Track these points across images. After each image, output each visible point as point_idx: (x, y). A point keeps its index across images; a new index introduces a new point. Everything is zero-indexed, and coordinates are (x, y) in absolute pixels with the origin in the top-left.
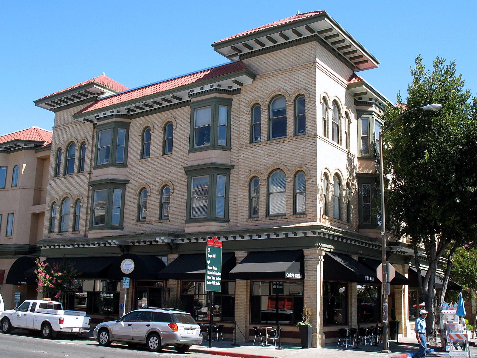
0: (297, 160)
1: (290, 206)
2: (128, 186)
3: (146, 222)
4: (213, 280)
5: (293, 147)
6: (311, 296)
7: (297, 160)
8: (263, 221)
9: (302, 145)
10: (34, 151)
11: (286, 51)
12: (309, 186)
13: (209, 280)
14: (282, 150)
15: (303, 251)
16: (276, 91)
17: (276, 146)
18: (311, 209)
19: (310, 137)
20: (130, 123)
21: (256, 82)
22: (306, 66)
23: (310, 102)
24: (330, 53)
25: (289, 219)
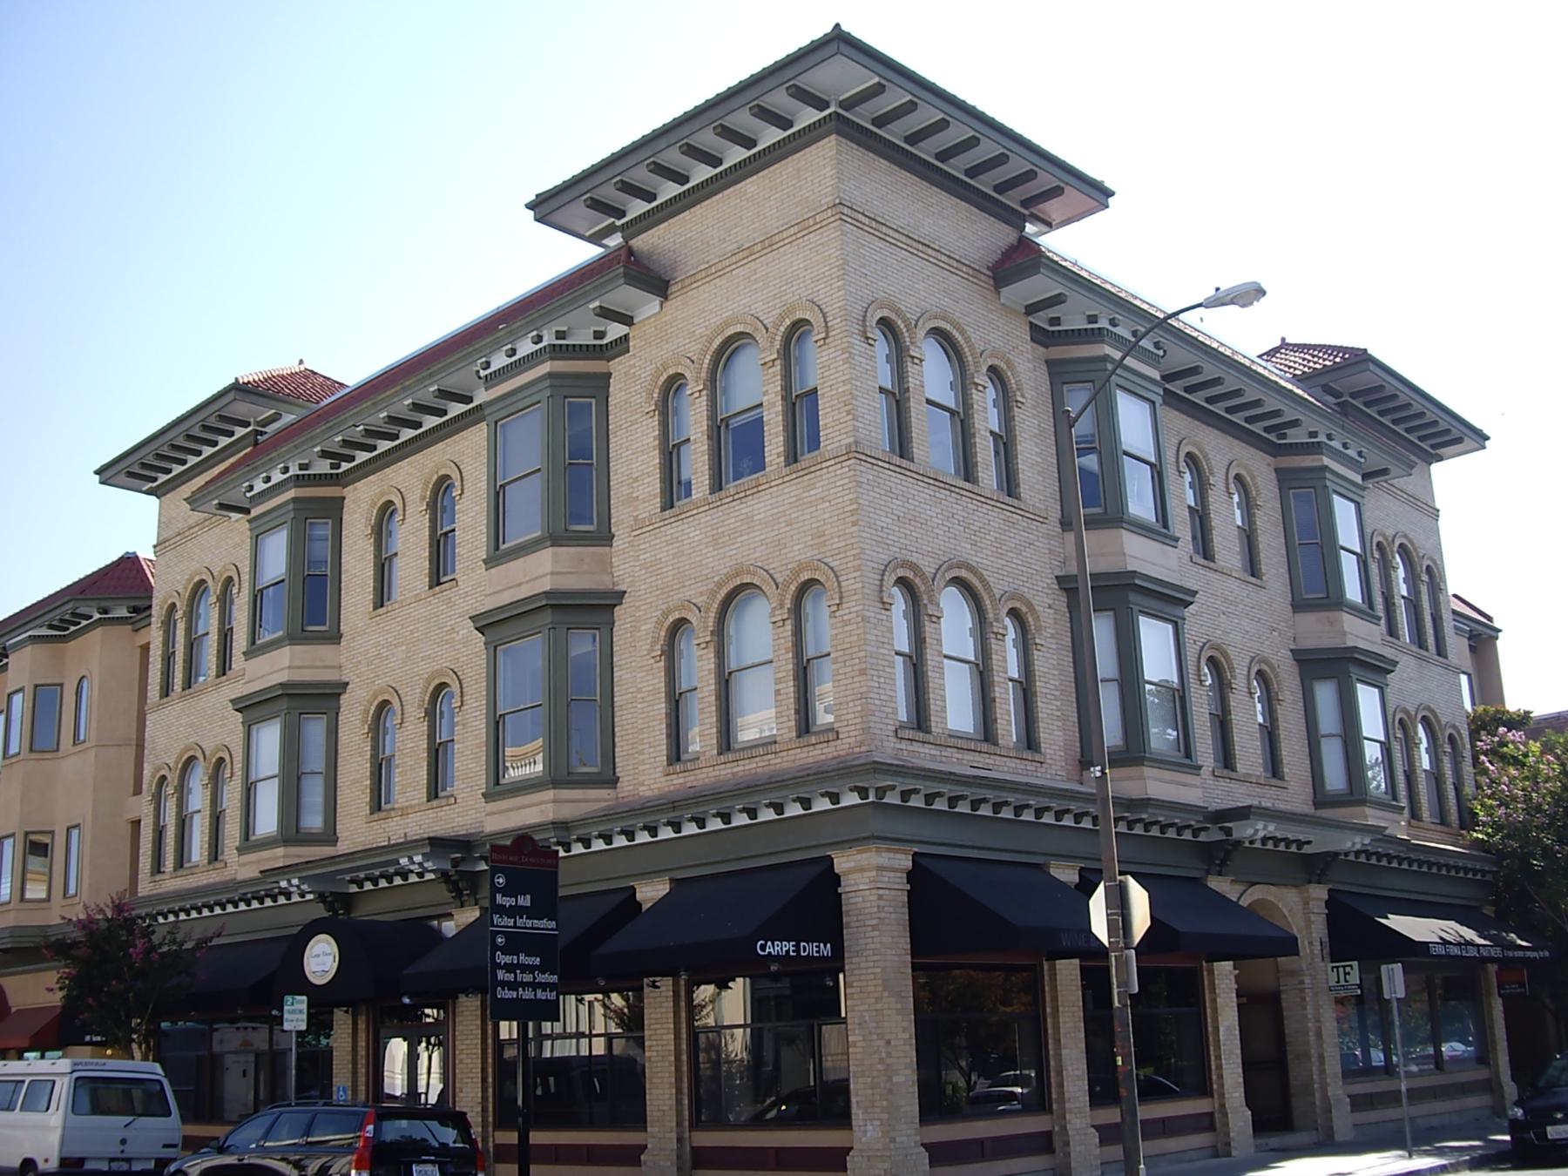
0: (798, 547)
1: (788, 709)
2: (344, 699)
3: (393, 814)
4: (524, 985)
5: (786, 502)
6: (867, 1018)
7: (798, 547)
8: (711, 769)
9: (812, 492)
10: (130, 627)
11: (751, 185)
12: (840, 630)
13: (504, 984)
14: (756, 518)
15: (832, 859)
16: (727, 324)
17: (737, 508)
18: (850, 711)
19: (832, 462)
20: (344, 498)
21: (671, 304)
22: (811, 222)
23: (827, 341)
24: (903, 171)
25: (785, 753)
